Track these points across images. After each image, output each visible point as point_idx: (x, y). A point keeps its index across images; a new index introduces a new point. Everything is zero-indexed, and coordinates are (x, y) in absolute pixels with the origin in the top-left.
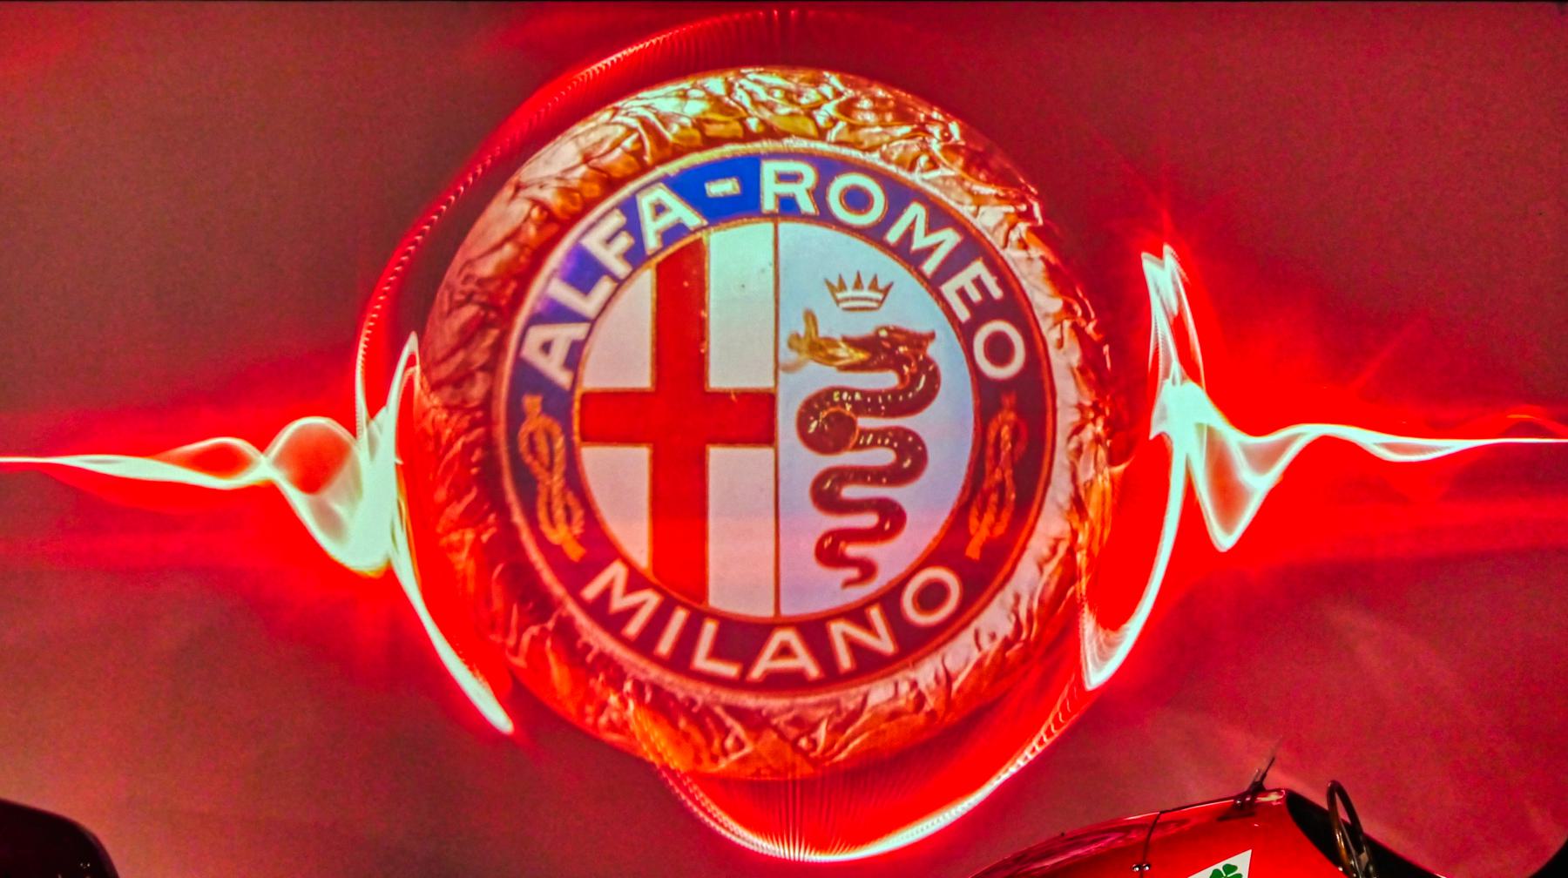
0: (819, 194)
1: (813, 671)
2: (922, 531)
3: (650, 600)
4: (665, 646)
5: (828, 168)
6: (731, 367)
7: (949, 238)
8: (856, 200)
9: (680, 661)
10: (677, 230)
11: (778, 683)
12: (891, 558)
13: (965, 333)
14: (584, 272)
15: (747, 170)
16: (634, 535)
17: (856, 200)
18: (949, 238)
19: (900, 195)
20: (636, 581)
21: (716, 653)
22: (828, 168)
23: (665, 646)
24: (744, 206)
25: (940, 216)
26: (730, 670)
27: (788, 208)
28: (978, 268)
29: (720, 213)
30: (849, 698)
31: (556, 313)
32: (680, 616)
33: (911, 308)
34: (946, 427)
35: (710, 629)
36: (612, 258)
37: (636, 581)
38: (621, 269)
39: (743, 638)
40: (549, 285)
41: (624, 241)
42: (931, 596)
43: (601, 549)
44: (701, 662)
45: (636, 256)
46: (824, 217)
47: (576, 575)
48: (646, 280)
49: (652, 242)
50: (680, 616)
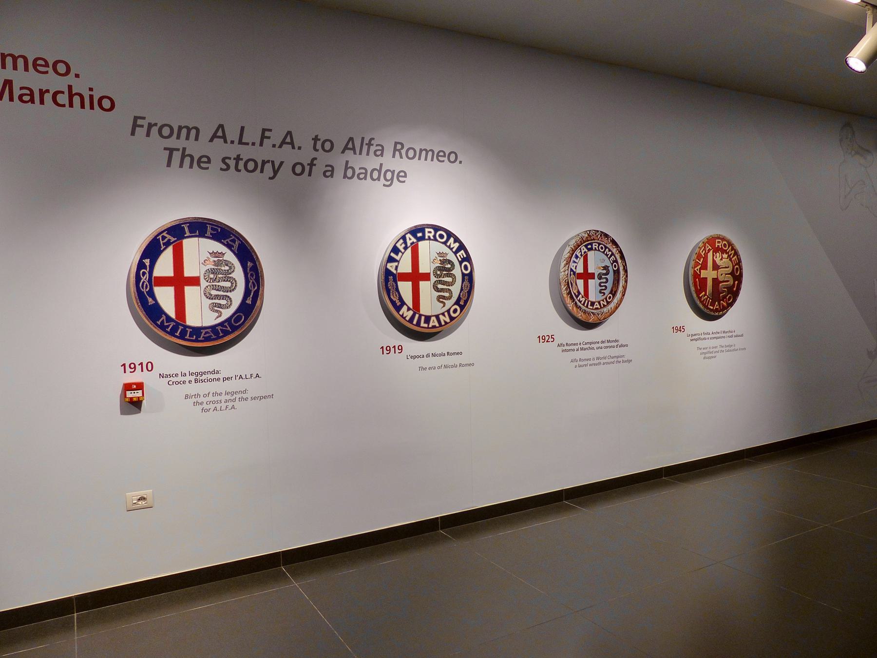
0: (435, 236)
1: (437, 325)
2: (454, 299)
3: (411, 313)
4: (415, 322)
5: (599, 244)
6: (424, 268)
7: (457, 245)
8: (441, 236)
9: (587, 307)
10: (413, 243)
11: (597, 309)
12: (449, 303)
13: (461, 263)
14: (577, 257)
15: (591, 244)
16: (408, 299)
17: (441, 236)
18: (457, 245)
19: (606, 248)
20: (409, 309)
21: (425, 322)
22: (599, 244)
23: (415, 322)
24: (423, 238)
25: (610, 250)
26: (426, 325)
27: (429, 239)
28: (462, 251)
29: (589, 250)
30: (602, 310)
31: (574, 262)
32: (417, 316)
33: (609, 264)
34: (610, 277)
35: (423, 318)
36: (579, 255)
37: (409, 309)
38: (403, 251)
39: (593, 304)
40: (573, 259)
41: (403, 245)
42: (455, 311)
43: (579, 293)
44: (422, 324)
45: (406, 248)
46: (435, 239)
47: (577, 297)
48: (409, 250)
49: (409, 244)
50: (417, 316)
